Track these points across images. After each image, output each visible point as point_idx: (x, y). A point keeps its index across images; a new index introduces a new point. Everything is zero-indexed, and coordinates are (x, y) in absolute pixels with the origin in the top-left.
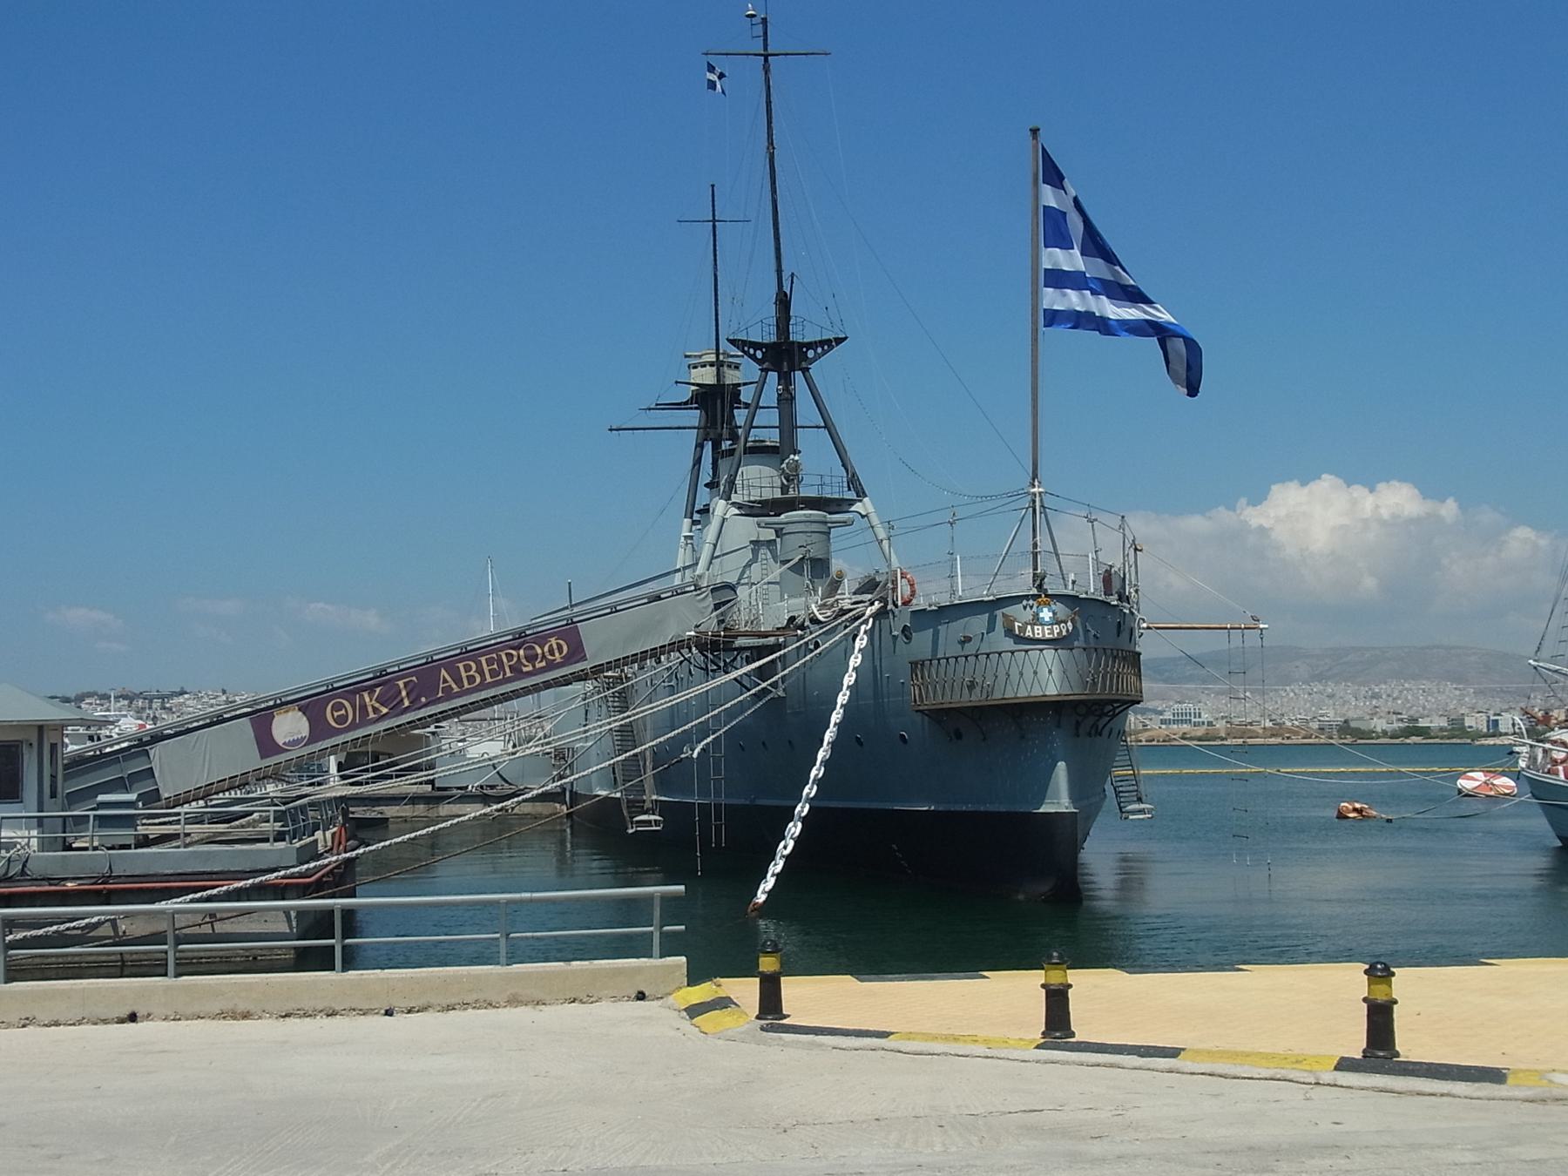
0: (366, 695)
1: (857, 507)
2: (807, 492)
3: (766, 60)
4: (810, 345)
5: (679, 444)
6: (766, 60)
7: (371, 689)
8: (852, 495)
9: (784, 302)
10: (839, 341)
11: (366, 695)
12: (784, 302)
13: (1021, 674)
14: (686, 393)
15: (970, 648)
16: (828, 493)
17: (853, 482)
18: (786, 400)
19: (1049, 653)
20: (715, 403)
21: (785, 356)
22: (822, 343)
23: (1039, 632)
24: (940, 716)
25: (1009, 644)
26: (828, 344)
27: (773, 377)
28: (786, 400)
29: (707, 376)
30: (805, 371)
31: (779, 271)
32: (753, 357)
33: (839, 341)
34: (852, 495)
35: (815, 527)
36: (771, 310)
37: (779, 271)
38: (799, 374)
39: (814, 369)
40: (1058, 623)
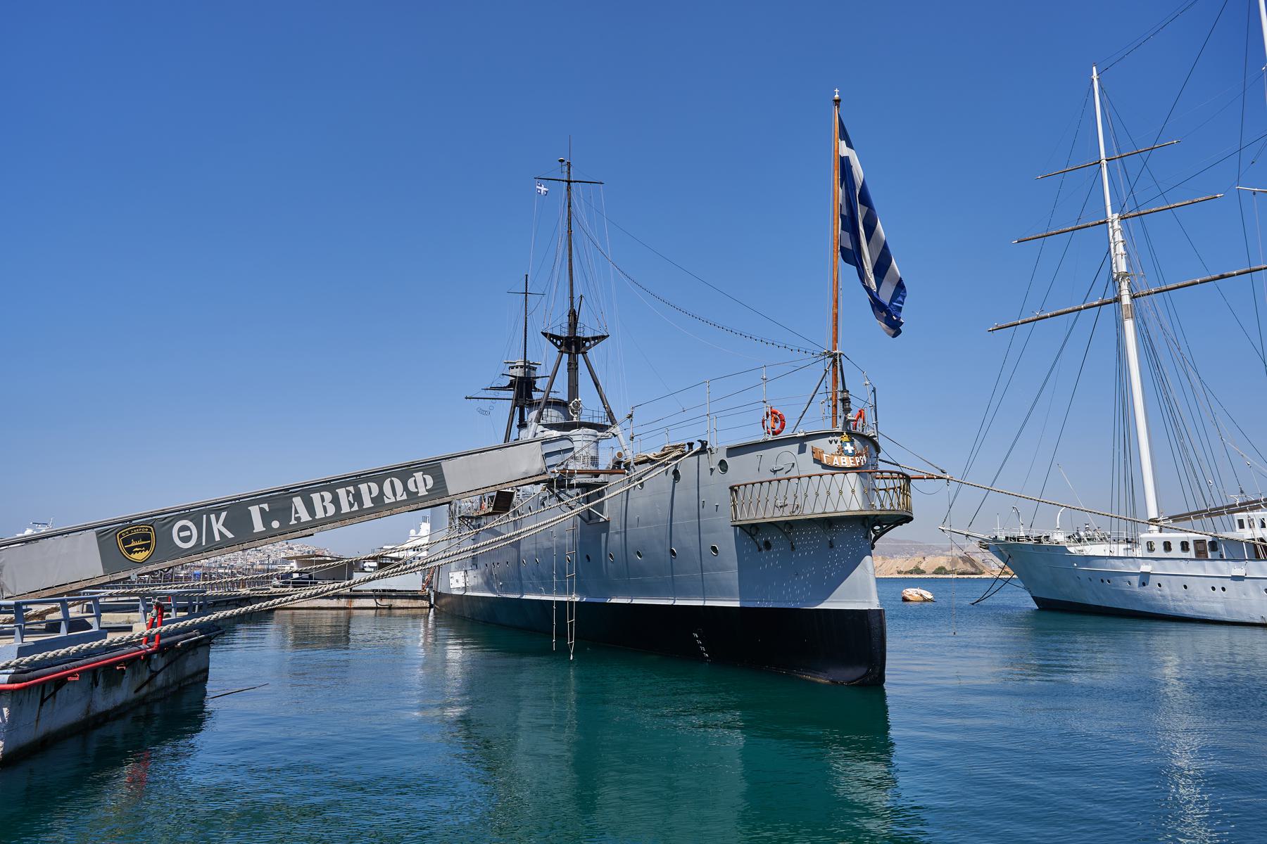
0: (213, 517)
1: (612, 430)
2: (584, 419)
3: (569, 188)
4: (587, 340)
5: (504, 407)
6: (569, 188)
7: (217, 512)
8: (609, 423)
9: (574, 316)
10: (604, 337)
11: (213, 517)
12: (574, 316)
13: (841, 492)
14: (506, 381)
15: (780, 475)
16: (596, 421)
17: (610, 414)
18: (573, 368)
19: (852, 476)
20: (523, 388)
21: (572, 345)
22: (594, 338)
23: (837, 461)
24: (749, 531)
25: (818, 469)
26: (551, 337)
27: (566, 356)
28: (573, 368)
29: (519, 373)
30: (584, 353)
31: (572, 298)
32: (555, 344)
33: (604, 337)
34: (609, 423)
35: (590, 438)
36: (566, 320)
37: (572, 298)
38: (580, 356)
39: (590, 353)
40: (858, 455)
